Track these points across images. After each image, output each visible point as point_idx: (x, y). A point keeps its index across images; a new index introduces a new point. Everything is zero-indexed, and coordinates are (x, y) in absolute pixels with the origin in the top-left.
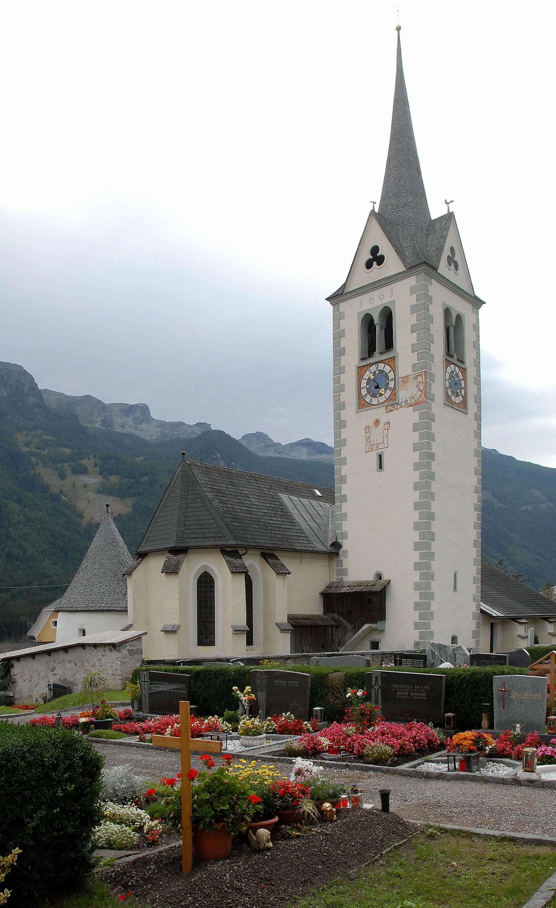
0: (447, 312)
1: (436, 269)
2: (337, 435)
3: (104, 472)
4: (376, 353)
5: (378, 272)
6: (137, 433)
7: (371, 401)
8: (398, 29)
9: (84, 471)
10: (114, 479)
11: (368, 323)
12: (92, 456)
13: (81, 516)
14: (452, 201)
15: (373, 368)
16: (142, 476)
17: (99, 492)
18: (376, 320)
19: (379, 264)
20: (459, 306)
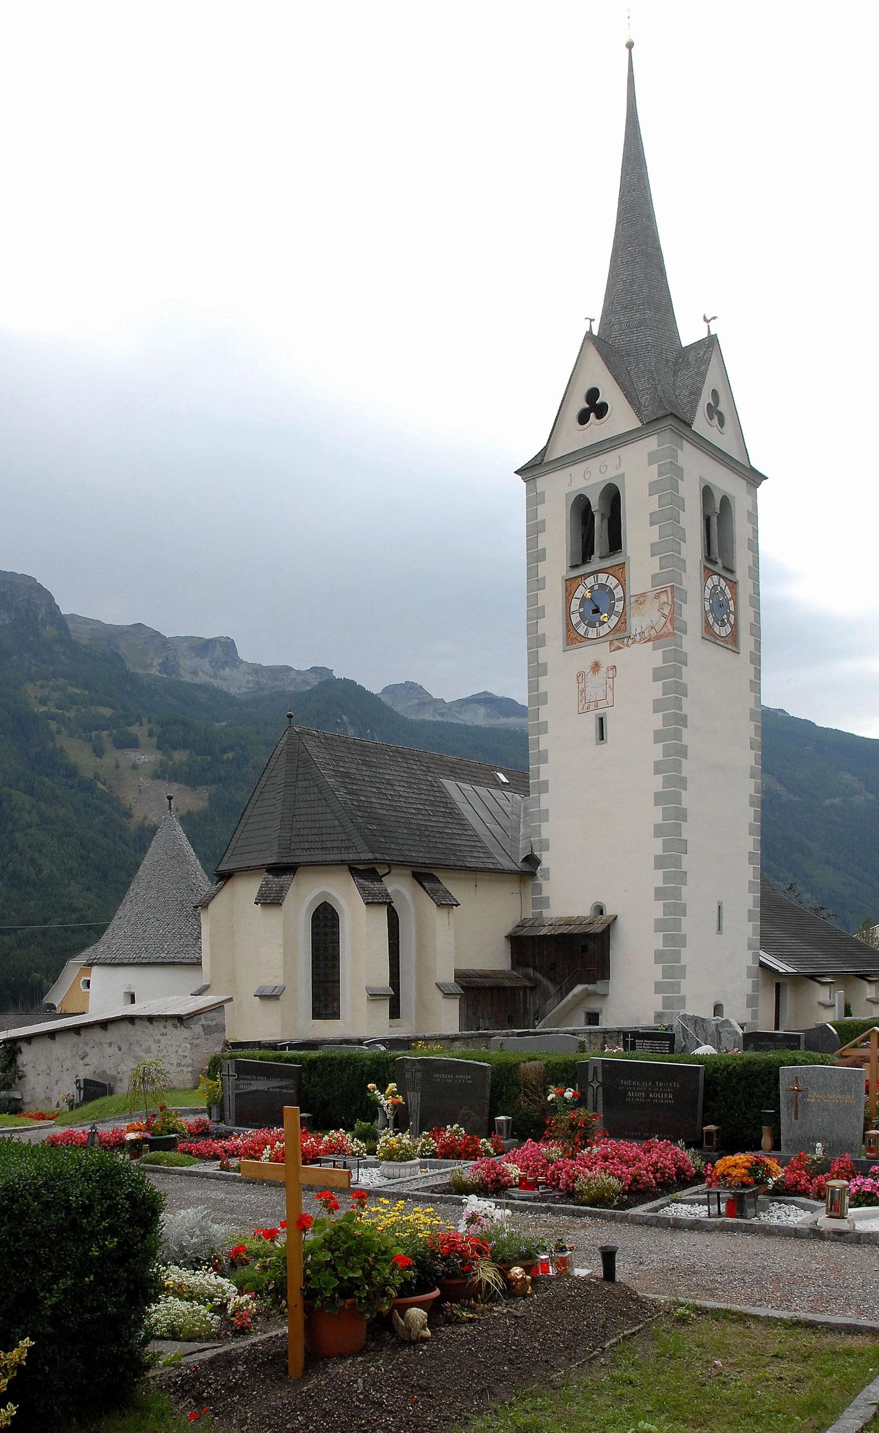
0: (707, 492)
1: (689, 425)
2: (533, 687)
3: (165, 744)
4: (595, 557)
5: (598, 430)
6: (217, 683)
7: (586, 632)
8: (630, 46)
9: (132, 744)
10: (180, 756)
11: (582, 510)
12: (145, 720)
13: (128, 815)
14: (714, 318)
15: (590, 581)
16: (224, 751)
17: (156, 776)
18: (595, 506)
19: (599, 417)
20: (726, 483)
